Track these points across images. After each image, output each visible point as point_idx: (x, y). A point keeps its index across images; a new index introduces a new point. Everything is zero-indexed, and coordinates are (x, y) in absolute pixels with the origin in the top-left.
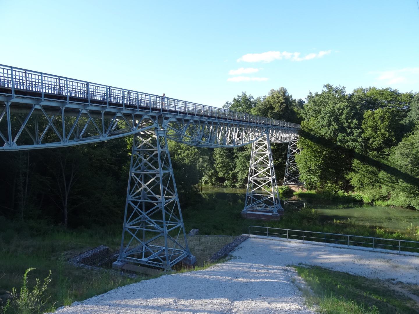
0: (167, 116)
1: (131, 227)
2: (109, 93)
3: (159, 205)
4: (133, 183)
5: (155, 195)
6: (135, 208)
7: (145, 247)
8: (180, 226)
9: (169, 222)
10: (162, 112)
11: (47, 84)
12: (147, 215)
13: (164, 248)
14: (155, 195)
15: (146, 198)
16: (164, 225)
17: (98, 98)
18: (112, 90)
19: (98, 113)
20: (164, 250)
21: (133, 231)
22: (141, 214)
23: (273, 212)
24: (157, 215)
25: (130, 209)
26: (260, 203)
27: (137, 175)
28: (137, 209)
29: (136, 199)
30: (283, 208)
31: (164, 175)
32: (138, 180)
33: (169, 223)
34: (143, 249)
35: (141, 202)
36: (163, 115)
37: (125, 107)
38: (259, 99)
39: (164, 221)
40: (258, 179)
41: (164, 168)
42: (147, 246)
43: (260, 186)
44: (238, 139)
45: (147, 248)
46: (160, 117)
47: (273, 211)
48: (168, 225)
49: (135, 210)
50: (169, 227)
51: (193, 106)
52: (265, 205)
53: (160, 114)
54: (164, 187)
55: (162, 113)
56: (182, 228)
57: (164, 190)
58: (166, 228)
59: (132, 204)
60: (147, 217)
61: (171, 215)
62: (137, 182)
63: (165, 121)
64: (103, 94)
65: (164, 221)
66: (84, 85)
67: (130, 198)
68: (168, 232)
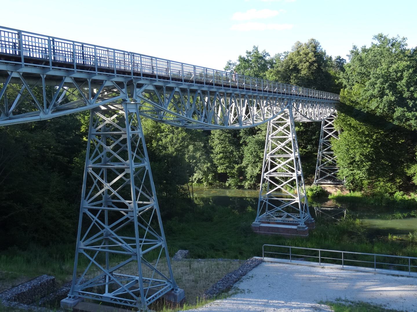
0: (140, 82)
1: (88, 248)
2: (52, 48)
3: (130, 214)
4: (90, 183)
5: (123, 200)
6: (94, 219)
7: (109, 277)
8: (161, 246)
9: (144, 240)
10: (132, 76)
11: (30, 46)
12: (112, 229)
13: (137, 278)
14: (123, 200)
15: (111, 204)
16: (137, 244)
17: (36, 55)
18: (57, 43)
19: (36, 77)
20: (137, 281)
21: (92, 253)
22: (103, 228)
23: (299, 224)
24: (127, 230)
25: (87, 221)
26: (279, 211)
27: (97, 170)
28: (96, 221)
29: (95, 206)
30: (313, 219)
31: (137, 170)
32: (98, 178)
33: (145, 242)
34: (105, 279)
35: (103, 211)
36: (134, 81)
37: (77, 69)
38: (278, 56)
39: (137, 238)
40: (276, 176)
41: (136, 160)
42: (112, 275)
43: (279, 187)
44: (247, 117)
45: (112, 278)
46: (130, 84)
47: (299, 223)
48: (142, 244)
49: (94, 222)
50: (144, 248)
51: (178, 68)
52: (286, 214)
53: (130, 79)
54: (137, 188)
55: (132, 78)
56: (164, 249)
57: (137, 192)
58: (141, 249)
59: (89, 213)
60: (112, 232)
61: (147, 230)
62: (97, 180)
63: (138, 89)
64: (44, 49)
65: (137, 238)
66: (79, 47)
67: (86, 205)
68: (144, 255)
